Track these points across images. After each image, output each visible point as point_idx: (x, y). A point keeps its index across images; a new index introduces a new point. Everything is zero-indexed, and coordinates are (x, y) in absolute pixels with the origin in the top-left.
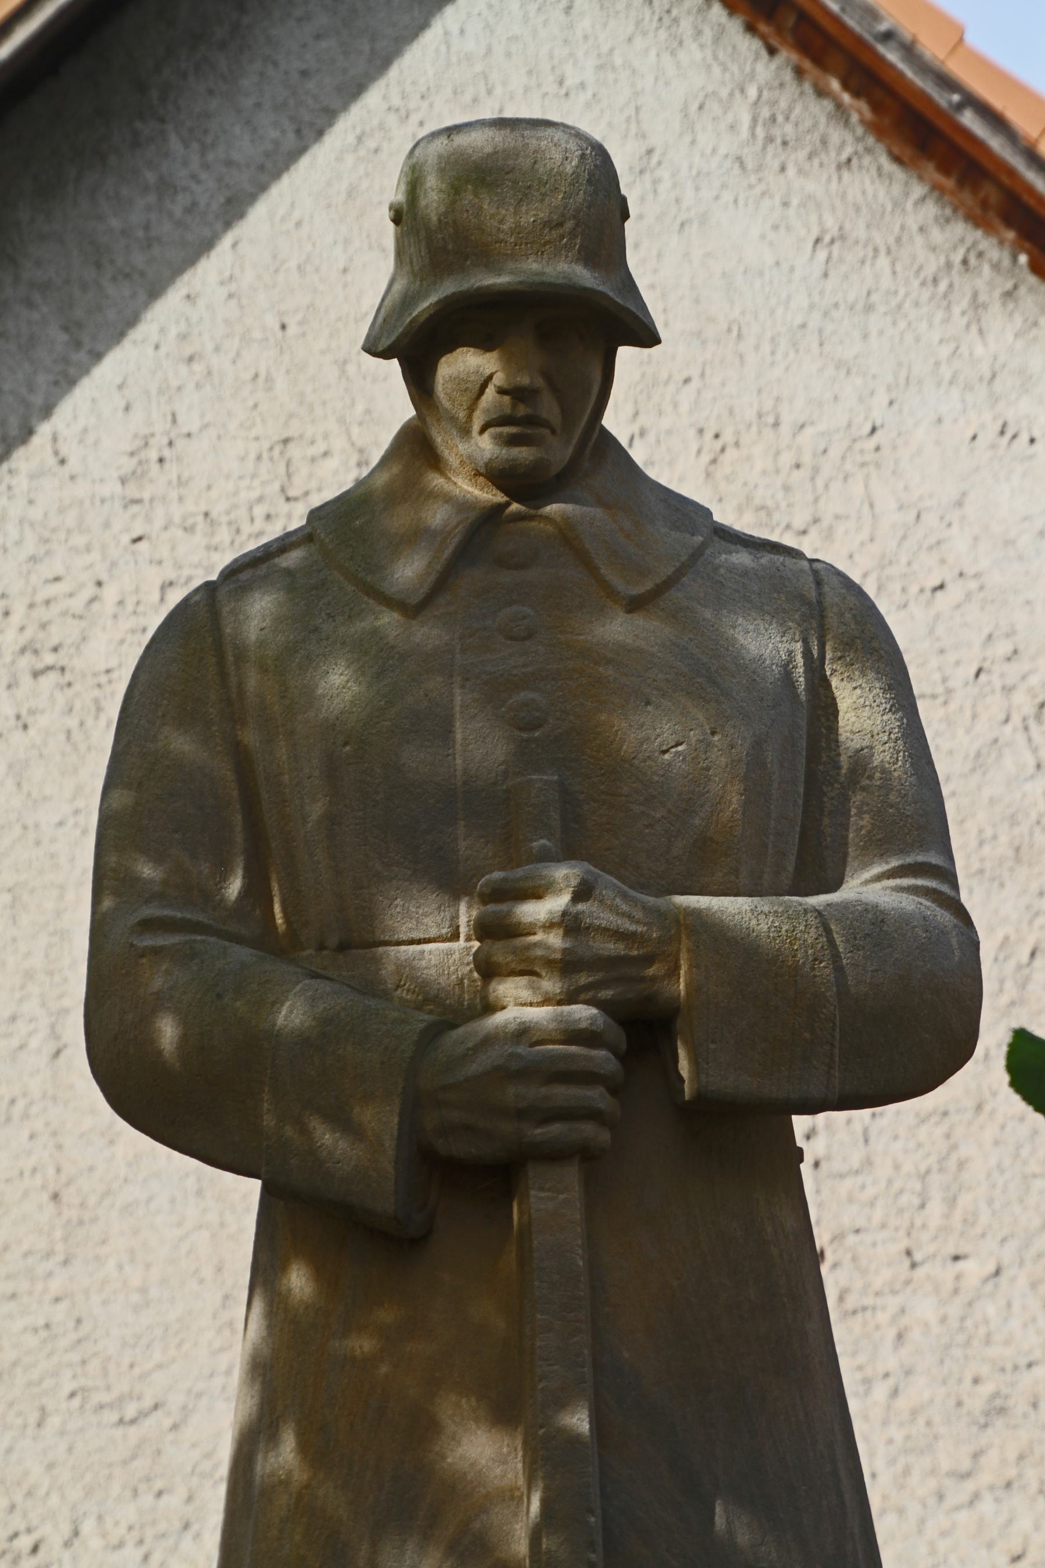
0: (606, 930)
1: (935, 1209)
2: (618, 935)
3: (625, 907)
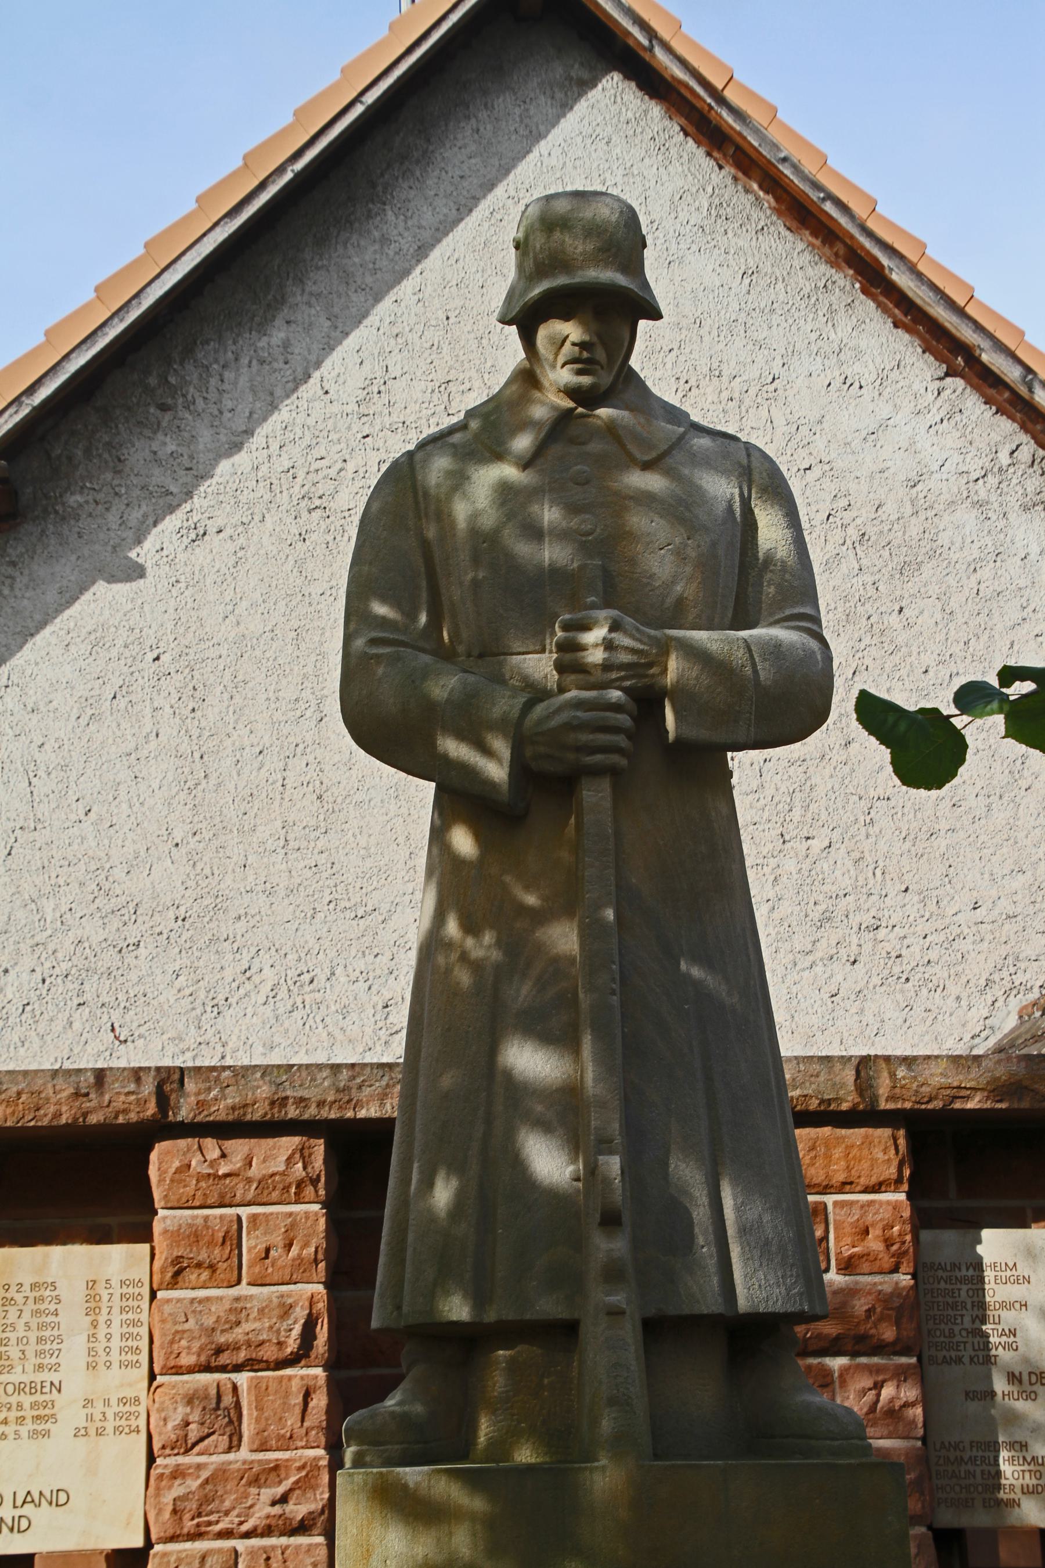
0: (627, 648)
1: (797, 813)
2: (633, 651)
3: (638, 635)
